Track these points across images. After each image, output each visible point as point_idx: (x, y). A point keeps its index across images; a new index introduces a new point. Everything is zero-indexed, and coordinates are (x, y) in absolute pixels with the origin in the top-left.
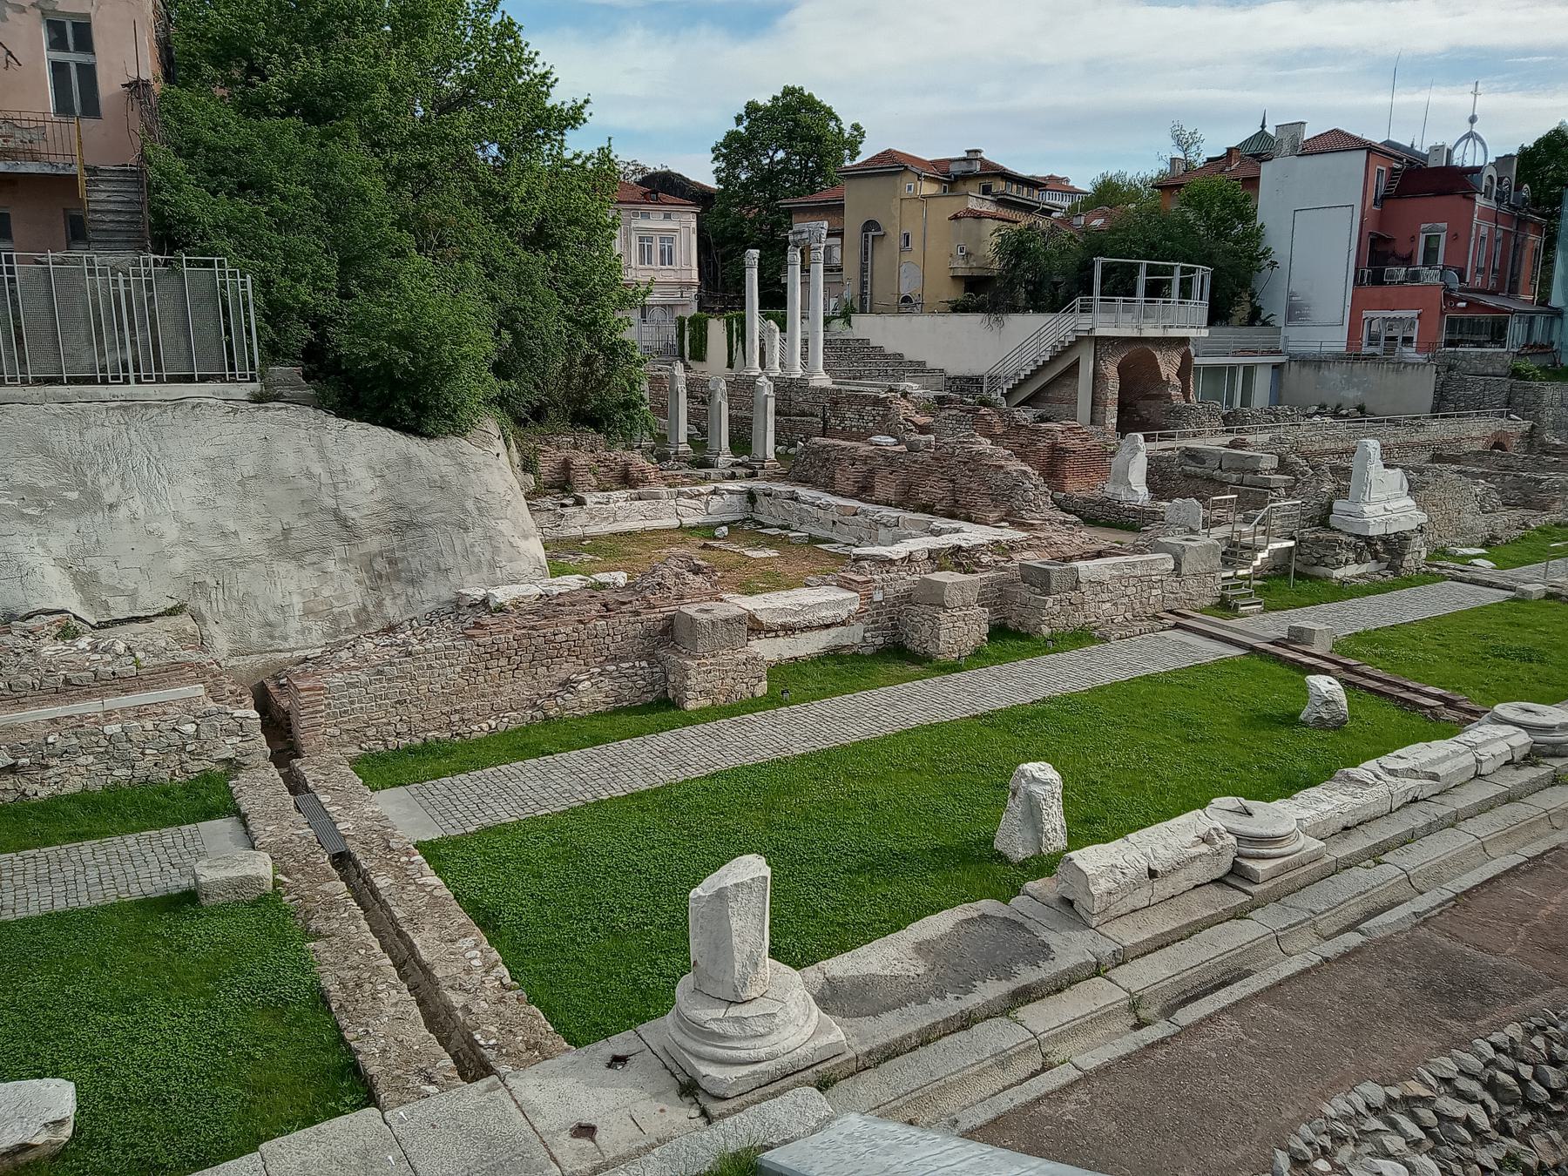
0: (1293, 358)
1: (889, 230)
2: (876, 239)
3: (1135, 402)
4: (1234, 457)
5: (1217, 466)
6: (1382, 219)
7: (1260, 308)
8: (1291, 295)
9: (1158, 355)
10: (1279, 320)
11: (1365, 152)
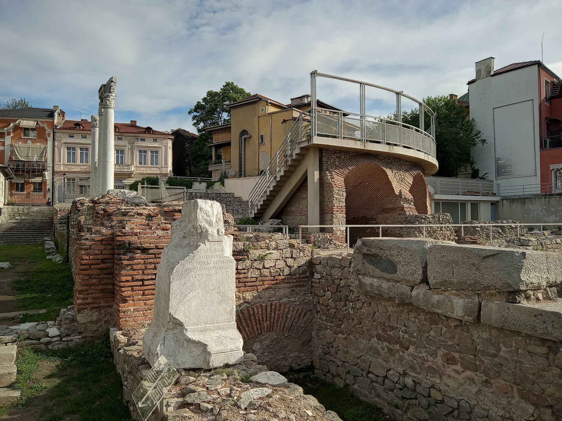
0: (504, 199)
1: (253, 134)
2: (247, 140)
3: (374, 217)
4: (388, 221)
5: (418, 276)
6: (551, 109)
7: (478, 170)
8: (497, 160)
9: (389, 172)
10: (492, 176)
11: (536, 66)
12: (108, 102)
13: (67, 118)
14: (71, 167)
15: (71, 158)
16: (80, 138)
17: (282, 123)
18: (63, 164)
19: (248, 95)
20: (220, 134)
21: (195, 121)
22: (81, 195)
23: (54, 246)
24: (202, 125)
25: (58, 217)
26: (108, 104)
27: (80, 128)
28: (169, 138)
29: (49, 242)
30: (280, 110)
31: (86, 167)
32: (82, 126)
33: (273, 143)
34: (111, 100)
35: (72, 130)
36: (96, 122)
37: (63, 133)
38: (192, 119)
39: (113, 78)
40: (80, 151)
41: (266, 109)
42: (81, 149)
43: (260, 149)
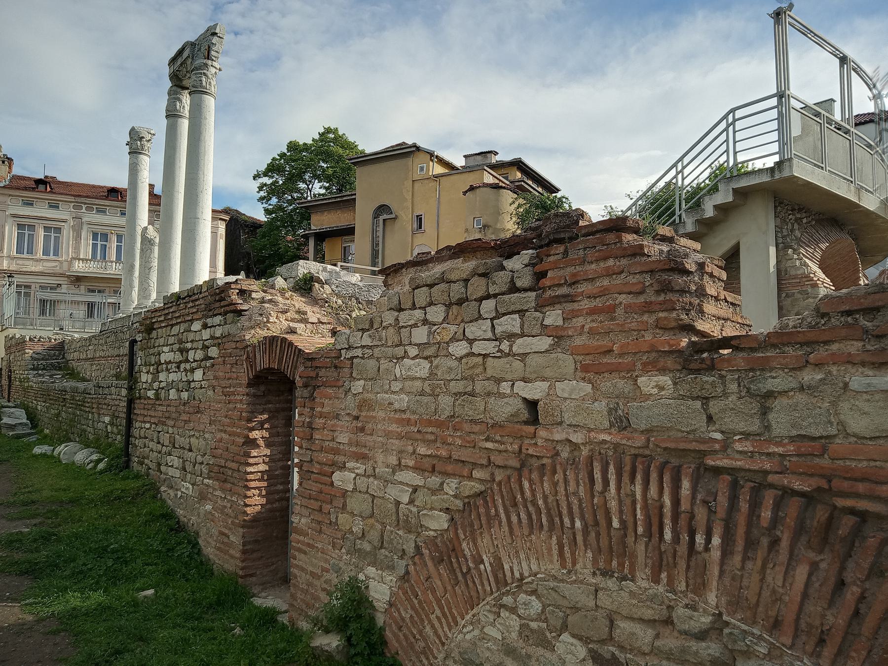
2: (388, 223)
12: (204, 79)
13: (17, 170)
14: (24, 262)
15: (25, 245)
16: (47, 207)
17: (465, 193)
18: (9, 257)
19: (362, 152)
20: (326, 213)
21: (262, 194)
22: (41, 317)
23: (25, 421)
24: (274, 200)
25: (26, 355)
26: (204, 84)
27: (46, 189)
28: (221, 219)
29: (12, 410)
30: (447, 171)
31: (54, 264)
32: (50, 186)
33: (442, 230)
34: (210, 76)
35: (30, 191)
36: (141, 141)
37: (10, 195)
38: (258, 190)
39: (218, 27)
40: (43, 233)
41: (428, 166)
42: (47, 229)
43: (415, 240)
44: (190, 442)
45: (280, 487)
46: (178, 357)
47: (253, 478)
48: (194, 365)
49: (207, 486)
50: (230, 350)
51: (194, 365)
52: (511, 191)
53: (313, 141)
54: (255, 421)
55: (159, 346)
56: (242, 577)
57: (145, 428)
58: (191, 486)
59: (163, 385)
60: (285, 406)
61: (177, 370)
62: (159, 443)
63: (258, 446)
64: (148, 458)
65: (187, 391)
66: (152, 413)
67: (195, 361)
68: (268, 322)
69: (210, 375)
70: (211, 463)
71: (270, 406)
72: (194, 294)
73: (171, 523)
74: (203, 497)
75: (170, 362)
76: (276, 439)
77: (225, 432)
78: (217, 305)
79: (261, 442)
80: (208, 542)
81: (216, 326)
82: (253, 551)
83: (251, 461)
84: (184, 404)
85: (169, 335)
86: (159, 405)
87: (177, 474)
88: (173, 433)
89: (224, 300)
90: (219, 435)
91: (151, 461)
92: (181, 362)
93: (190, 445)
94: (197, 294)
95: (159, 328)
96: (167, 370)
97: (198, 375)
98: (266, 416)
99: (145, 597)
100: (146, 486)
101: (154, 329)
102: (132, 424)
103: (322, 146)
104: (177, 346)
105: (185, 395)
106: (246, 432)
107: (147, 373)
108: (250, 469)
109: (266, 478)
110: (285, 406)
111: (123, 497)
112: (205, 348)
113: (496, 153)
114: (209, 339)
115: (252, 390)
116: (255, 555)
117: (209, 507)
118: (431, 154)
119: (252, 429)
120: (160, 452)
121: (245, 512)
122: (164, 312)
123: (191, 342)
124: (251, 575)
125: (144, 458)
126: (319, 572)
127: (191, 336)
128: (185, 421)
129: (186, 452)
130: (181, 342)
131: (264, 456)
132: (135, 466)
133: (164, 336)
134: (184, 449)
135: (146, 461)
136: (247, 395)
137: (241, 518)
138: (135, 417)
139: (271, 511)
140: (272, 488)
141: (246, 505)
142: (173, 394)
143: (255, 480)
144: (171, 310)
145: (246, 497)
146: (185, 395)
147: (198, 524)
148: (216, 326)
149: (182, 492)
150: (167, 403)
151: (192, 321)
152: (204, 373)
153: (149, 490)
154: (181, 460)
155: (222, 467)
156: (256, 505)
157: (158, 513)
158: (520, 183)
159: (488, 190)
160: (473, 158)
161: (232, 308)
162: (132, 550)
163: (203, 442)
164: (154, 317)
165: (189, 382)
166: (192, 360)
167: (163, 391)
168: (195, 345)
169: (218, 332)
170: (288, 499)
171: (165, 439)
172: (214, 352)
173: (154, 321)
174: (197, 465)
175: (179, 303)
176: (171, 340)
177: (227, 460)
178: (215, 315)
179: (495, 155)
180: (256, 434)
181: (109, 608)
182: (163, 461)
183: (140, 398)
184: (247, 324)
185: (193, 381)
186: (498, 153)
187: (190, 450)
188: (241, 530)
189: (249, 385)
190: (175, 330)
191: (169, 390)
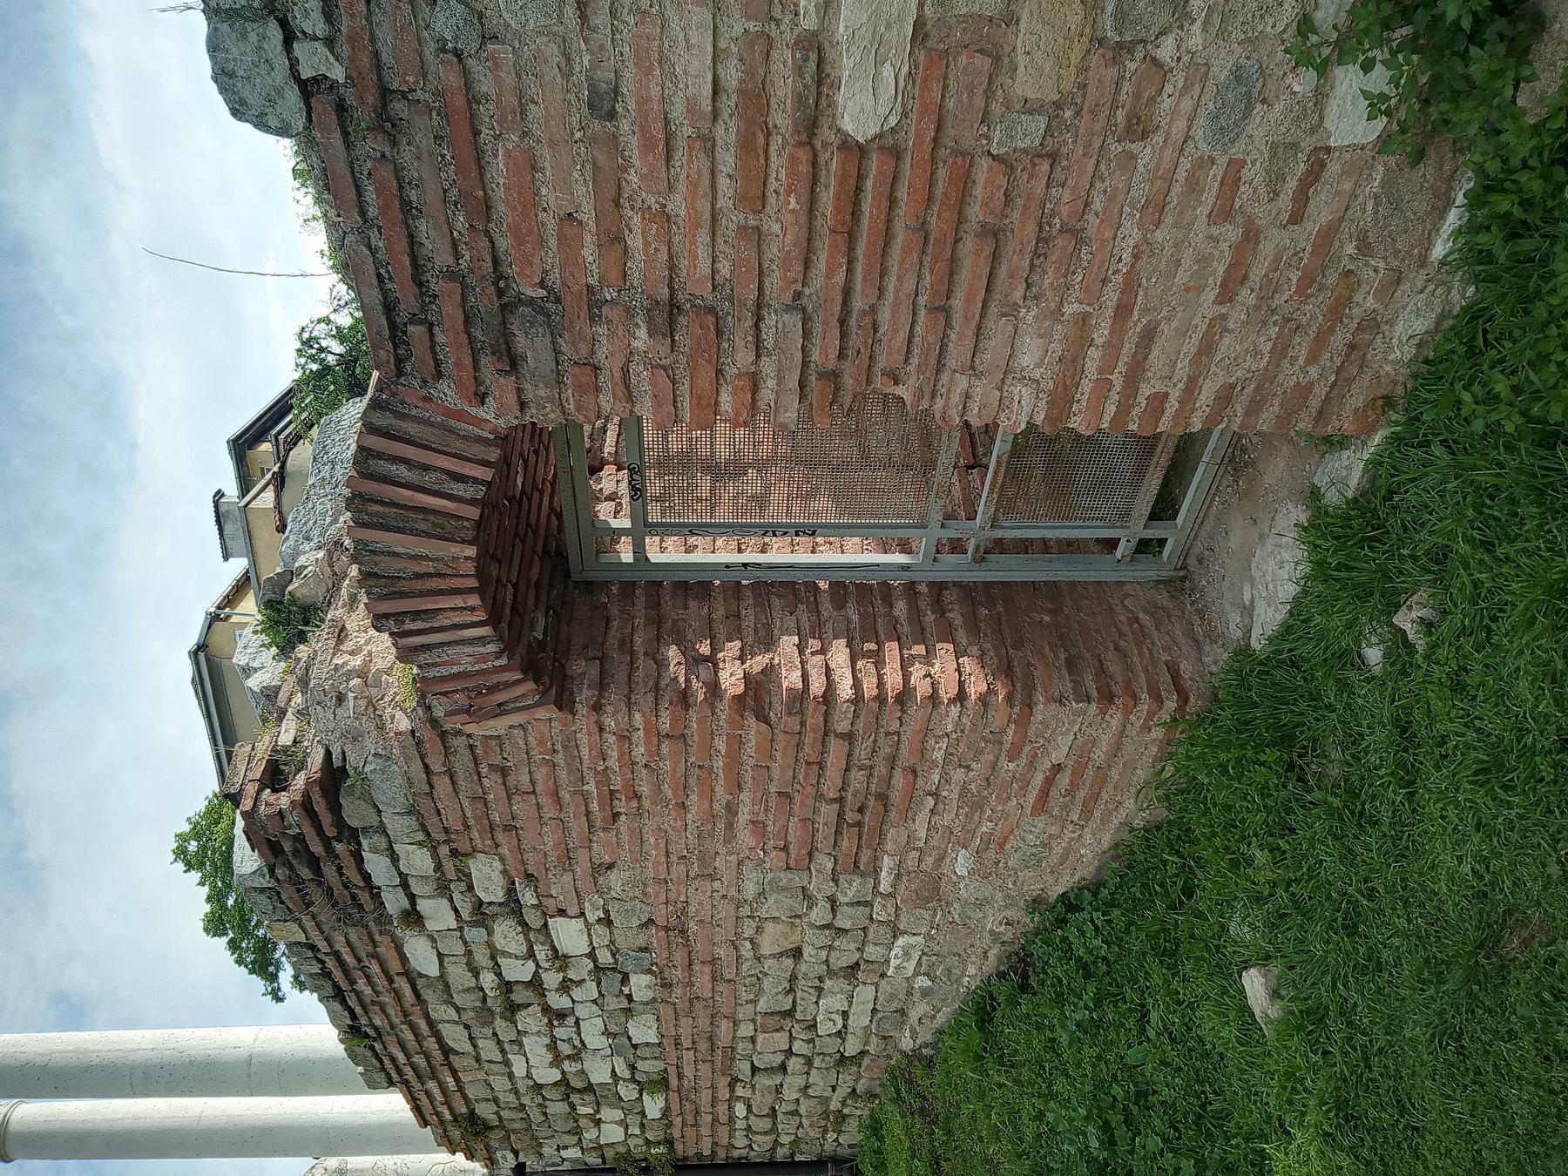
44: (773, 956)
45: (901, 608)
46: (530, 1019)
47: (875, 680)
48: (542, 953)
49: (898, 876)
50: (466, 804)
51: (542, 953)
52: (291, 449)
53: (204, 885)
54: (687, 680)
55: (517, 1093)
56: (1184, 699)
57: (746, 1118)
58: (901, 941)
59: (622, 1070)
60: (641, 602)
61: (570, 1020)
62: (783, 1068)
63: (769, 670)
64: (827, 1100)
65: (625, 979)
66: (706, 1095)
67: (531, 955)
68: (362, 673)
69: (560, 887)
70: (830, 865)
71: (638, 641)
72: (327, 975)
73: (1002, 991)
74: (931, 892)
75: (553, 1046)
76: (749, 619)
77: (731, 811)
78: (329, 871)
79: (757, 663)
80: (1063, 860)
81: (401, 874)
82: (1102, 673)
83: (817, 686)
84: (667, 985)
85: (478, 1060)
86: (680, 1077)
87: (865, 993)
88: (753, 1021)
89: (300, 839)
90: (746, 838)
91: (834, 1089)
92: (546, 1009)
93: (781, 954)
94: (322, 962)
95: (465, 1097)
96: (575, 1057)
97: (569, 935)
98: (673, 653)
99: (1275, 994)
100: (898, 1092)
101: (472, 1113)
102: (740, 1158)
103: (213, 863)
104: (500, 1025)
105: (640, 985)
106: (724, 710)
107: (598, 1122)
108: (845, 690)
109: (873, 646)
110: (641, 602)
111: (933, 1151)
112: (481, 915)
113: (219, 494)
114: (451, 900)
115: (584, 695)
116: (1114, 668)
117: (962, 863)
118: (214, 619)
119: (714, 688)
120: (809, 1062)
121: (984, 700)
122: (416, 1085)
123: (476, 975)
124: (1176, 676)
125: (825, 1114)
126: (1232, 233)
127: (459, 975)
128: (714, 979)
129: (803, 968)
130: (485, 1014)
131: (801, 653)
132: (851, 1135)
133: (481, 1076)
134: (793, 979)
135: (834, 1105)
136: (597, 708)
137: (998, 717)
138: (722, 1154)
139: (973, 627)
140: (905, 629)
141: (961, 696)
142: (643, 1031)
143: (880, 677)
144: (401, 1058)
145: (934, 698)
146: (640, 985)
147: (1010, 902)
148: (401, 874)
149: (916, 973)
150: (670, 1048)
151: (411, 976)
152: (562, 912)
153: (910, 1081)
154: (828, 984)
155: (841, 815)
156: (958, 670)
157: (977, 1037)
158: (281, 442)
159: (287, 495)
160: (229, 542)
161: (320, 805)
162: (1099, 1084)
163: (771, 901)
164: (437, 1114)
165: (599, 970)
166: (531, 965)
167: (640, 1065)
168: (482, 958)
169: (418, 861)
170: (938, 588)
171: (770, 1047)
172: (487, 877)
173: (448, 1116)
174: (839, 923)
175: (371, 1032)
176: (489, 1050)
177: (820, 797)
178: (367, 878)
179: (223, 495)
180: (731, 678)
181: (1340, 1104)
182: (832, 1046)
183: (669, 1142)
184: (370, 744)
185: (592, 955)
186: (219, 491)
187: (797, 953)
188: (1040, 711)
189: (564, 703)
190: (455, 1037)
191: (635, 1047)
